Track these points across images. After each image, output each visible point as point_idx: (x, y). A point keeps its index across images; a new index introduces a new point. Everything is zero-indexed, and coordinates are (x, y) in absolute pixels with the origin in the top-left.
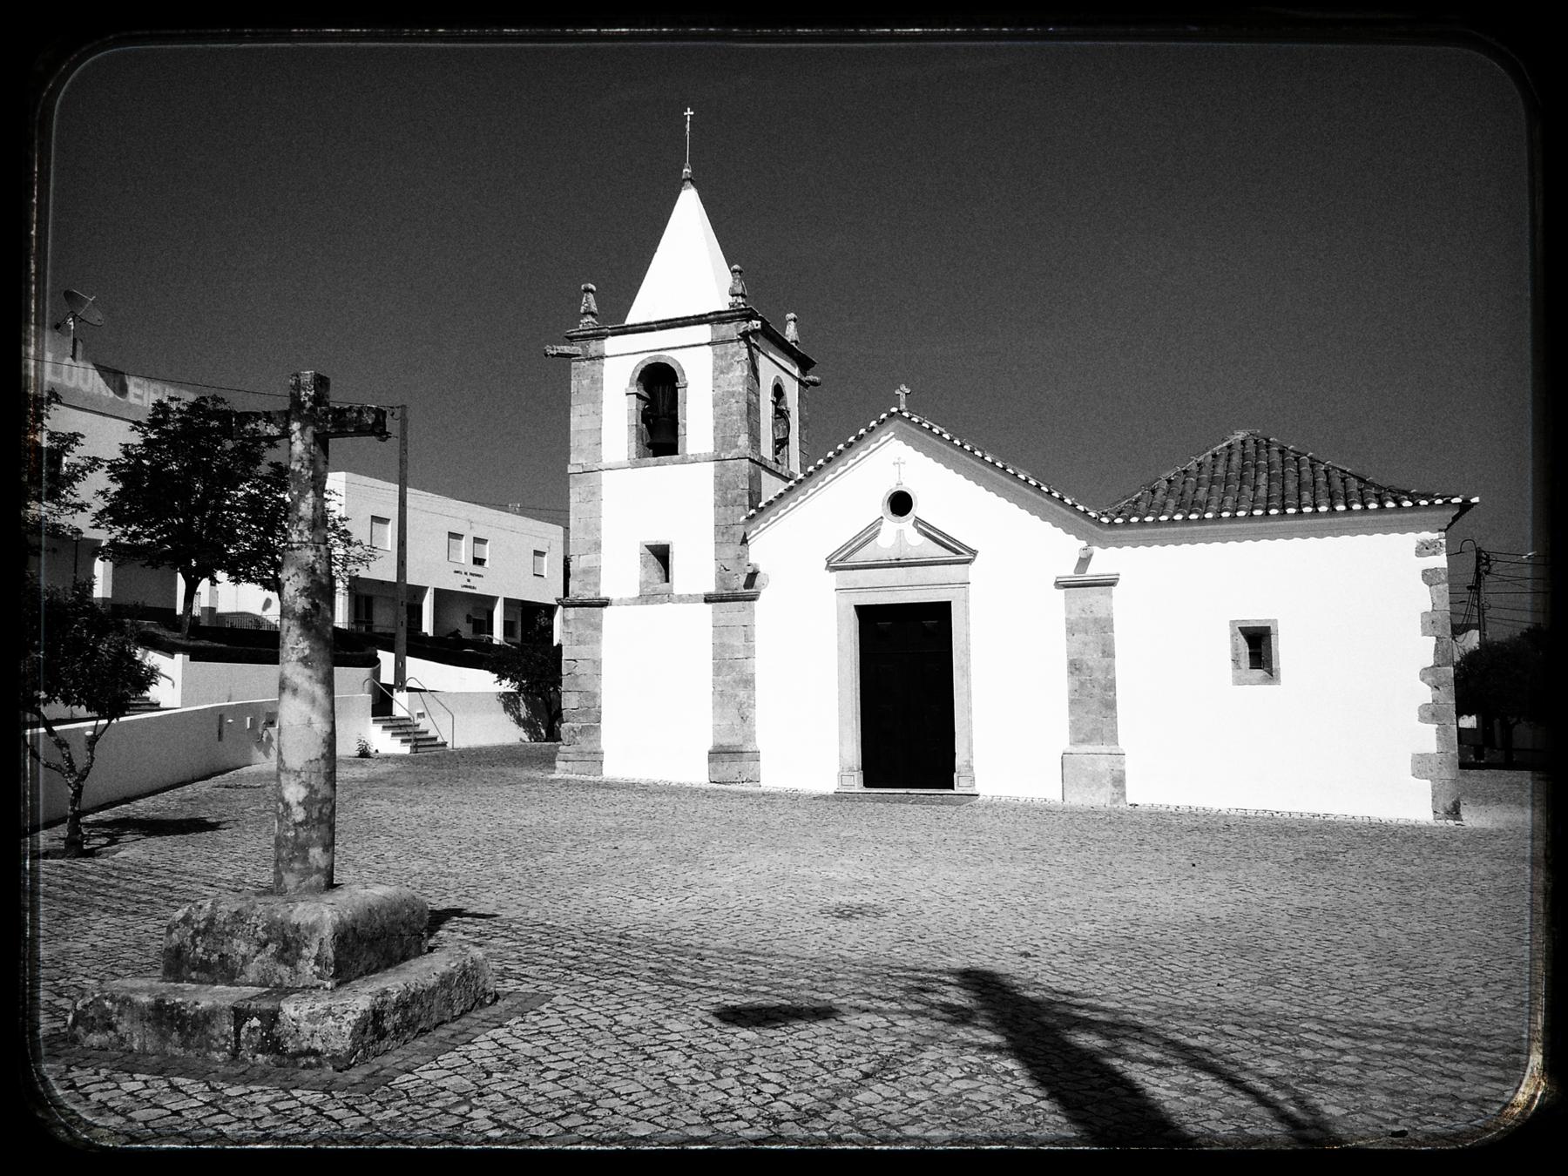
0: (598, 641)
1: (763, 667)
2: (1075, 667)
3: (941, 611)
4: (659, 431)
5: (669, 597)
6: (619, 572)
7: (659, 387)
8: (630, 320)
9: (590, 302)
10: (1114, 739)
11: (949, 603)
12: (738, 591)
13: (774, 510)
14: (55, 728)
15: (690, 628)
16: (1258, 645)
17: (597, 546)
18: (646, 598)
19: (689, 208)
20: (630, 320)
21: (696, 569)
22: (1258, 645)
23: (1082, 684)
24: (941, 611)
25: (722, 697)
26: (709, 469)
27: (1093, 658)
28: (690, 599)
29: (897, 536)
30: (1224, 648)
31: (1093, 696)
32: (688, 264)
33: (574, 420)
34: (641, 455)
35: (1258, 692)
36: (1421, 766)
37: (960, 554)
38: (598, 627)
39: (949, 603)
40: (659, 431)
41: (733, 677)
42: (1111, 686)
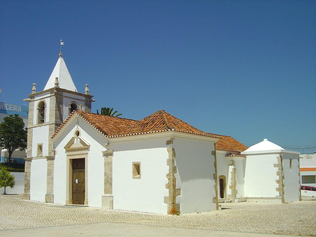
0: (30, 168)
8: (45, 89)
9: (34, 88)
16: (137, 168)
22: (137, 168)
30: (130, 168)
37: (86, 147)
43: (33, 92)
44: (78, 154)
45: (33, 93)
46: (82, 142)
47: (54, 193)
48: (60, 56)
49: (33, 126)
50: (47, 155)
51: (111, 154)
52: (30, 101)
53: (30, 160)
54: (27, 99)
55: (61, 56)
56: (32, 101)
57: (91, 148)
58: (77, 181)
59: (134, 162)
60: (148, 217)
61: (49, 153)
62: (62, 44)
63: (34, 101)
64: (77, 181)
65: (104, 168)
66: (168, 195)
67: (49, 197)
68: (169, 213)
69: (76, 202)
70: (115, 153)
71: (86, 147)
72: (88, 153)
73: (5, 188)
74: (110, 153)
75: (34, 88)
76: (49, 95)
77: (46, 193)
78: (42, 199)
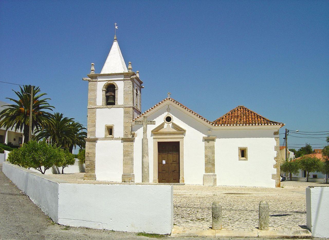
0: (95, 149)
2: (206, 156)
3: (178, 143)
4: (110, 100)
6: (100, 132)
7: (111, 89)
8: (102, 73)
9: (93, 68)
10: (214, 172)
12: (128, 140)
13: (225, 236)
14: (81, 128)
15: (117, 147)
16: (243, 153)
17: (95, 126)
18: (105, 138)
19: (115, 46)
21: (119, 132)
22: (243, 153)
23: (208, 160)
24: (178, 143)
25: (125, 164)
26: (122, 110)
27: (210, 154)
29: (168, 127)
30: (237, 153)
31: (210, 164)
32: (115, 62)
33: (89, 95)
34: (246, 149)
35: (243, 162)
36: (273, 177)
37: (182, 132)
38: (95, 145)
40: (110, 100)
41: (128, 156)
42: (214, 160)
43: (92, 72)
44: (170, 138)
45: (92, 73)
46: (175, 126)
47: (134, 173)
48: (115, 39)
49: (96, 107)
50: (122, 136)
51: (213, 140)
52: (89, 81)
53: (95, 140)
55: (116, 39)
56: (91, 82)
57: (187, 133)
58: (164, 162)
59: (240, 147)
60: (272, 189)
61: (125, 135)
62: (116, 27)
63: (96, 81)
64: (164, 162)
65: (204, 151)
66: (275, 173)
68: (277, 186)
69: (163, 181)
70: (217, 140)
71: (182, 132)
72: (184, 138)
73: (63, 168)
74: (211, 138)
75: (93, 68)
76: (122, 79)
77: (122, 174)
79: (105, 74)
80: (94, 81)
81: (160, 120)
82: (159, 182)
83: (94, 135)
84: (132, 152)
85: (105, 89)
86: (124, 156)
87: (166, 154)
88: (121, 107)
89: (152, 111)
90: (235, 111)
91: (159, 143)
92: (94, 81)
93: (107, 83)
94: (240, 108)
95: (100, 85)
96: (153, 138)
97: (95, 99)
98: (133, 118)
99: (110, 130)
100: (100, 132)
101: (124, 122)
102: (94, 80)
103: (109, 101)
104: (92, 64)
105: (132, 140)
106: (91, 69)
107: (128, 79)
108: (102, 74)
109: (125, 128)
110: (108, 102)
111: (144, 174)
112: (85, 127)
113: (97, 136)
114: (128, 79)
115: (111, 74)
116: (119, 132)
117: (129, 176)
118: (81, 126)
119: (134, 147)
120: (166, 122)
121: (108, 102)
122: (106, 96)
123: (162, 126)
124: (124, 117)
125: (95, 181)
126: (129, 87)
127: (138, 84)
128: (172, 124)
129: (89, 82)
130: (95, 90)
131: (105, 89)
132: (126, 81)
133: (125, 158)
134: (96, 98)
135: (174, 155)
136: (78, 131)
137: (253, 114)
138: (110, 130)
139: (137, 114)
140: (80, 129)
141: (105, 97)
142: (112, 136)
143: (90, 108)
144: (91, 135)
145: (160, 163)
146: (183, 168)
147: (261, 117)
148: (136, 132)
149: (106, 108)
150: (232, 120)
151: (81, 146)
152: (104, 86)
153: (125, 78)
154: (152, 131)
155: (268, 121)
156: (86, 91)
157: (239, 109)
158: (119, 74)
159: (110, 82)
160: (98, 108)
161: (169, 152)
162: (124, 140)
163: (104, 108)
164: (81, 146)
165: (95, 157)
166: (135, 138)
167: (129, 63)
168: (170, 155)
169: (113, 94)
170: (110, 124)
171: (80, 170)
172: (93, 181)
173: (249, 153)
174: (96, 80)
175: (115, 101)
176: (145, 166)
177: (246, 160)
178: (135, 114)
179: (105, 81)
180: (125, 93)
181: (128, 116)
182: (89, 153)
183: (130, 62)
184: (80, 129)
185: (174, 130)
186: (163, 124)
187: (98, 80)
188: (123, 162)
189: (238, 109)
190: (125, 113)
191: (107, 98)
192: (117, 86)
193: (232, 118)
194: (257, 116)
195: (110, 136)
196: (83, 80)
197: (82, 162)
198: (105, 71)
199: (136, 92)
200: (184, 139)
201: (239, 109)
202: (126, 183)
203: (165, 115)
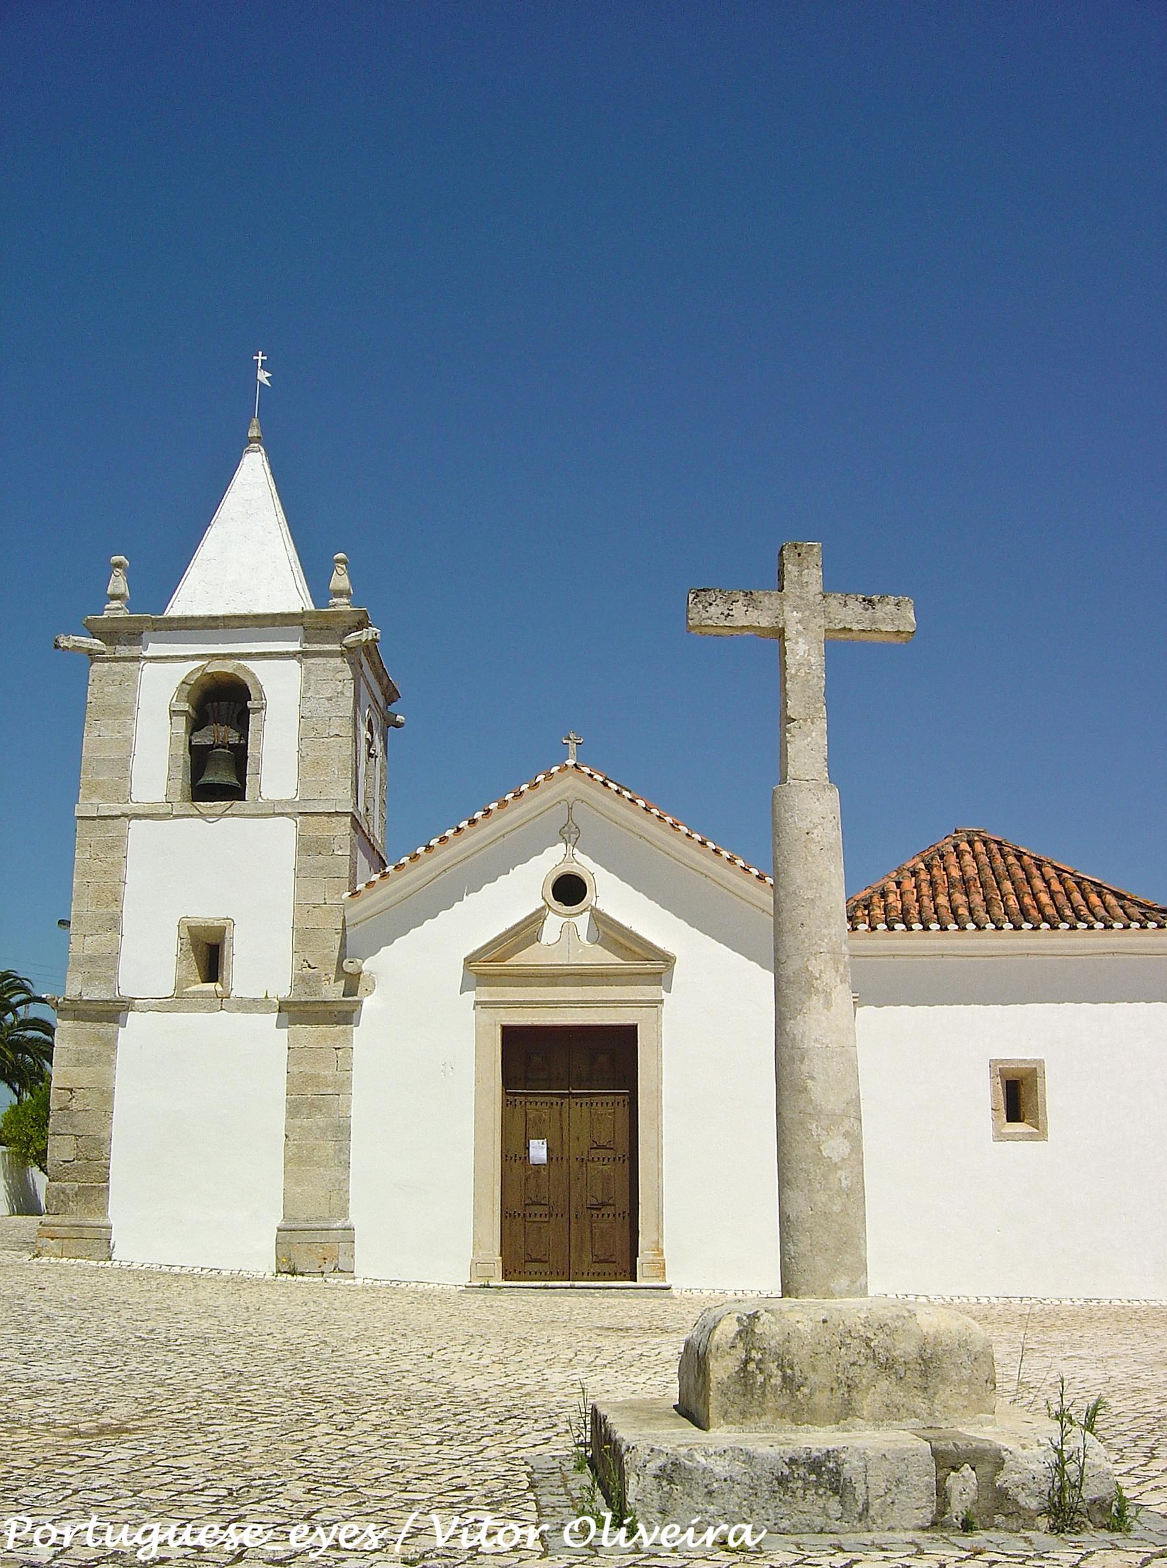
0: (111, 1062)
1: (364, 1107)
3: (627, 1036)
4: (217, 768)
5: (222, 1001)
6: (149, 960)
7: (221, 707)
8: (178, 607)
9: (118, 584)
11: (634, 1028)
12: (323, 1009)
15: (246, 1052)
16: (1018, 1096)
17: (114, 923)
18: (178, 1001)
19: (253, 474)
20: (178, 607)
21: (263, 961)
22: (1018, 1096)
24: (627, 1036)
25: (298, 1159)
26: (285, 831)
28: (249, 1005)
29: (564, 937)
30: (985, 1095)
32: (246, 553)
33: (89, 737)
35: (1020, 1151)
37: (650, 965)
38: (111, 1043)
39: (634, 1028)
40: (217, 768)
41: (317, 1116)
43: (115, 604)
44: (578, 1002)
45: (115, 610)
46: (609, 932)
47: (353, 1219)
50: (282, 989)
52: (93, 656)
53: (113, 1012)
54: (89, 640)
55: (257, 440)
56: (108, 660)
57: (679, 972)
58: (538, 1151)
61: (301, 980)
62: (263, 376)
63: (136, 659)
64: (538, 1151)
67: (311, 1243)
71: (650, 965)
75: (118, 584)
76: (295, 647)
77: (278, 1220)
78: (248, 1244)
79: (193, 618)
80: (125, 659)
81: (522, 890)
82: (505, 1277)
83: (111, 979)
84: (343, 1086)
85: (186, 707)
86: (294, 1110)
87: (547, 1099)
88: (282, 814)
89: (472, 839)
90: (942, 857)
91: (512, 1036)
92: (125, 659)
93: (197, 669)
94: (971, 843)
95: (157, 687)
96: (477, 1003)
97: (123, 765)
98: (353, 882)
99: (209, 954)
100: (149, 960)
101: (297, 905)
102: (123, 651)
103: (208, 778)
104: (116, 559)
105: (344, 1015)
106: (108, 592)
107: (328, 647)
108: (172, 619)
109: (303, 937)
110: (202, 781)
111: (822, 1197)
112: (44, 996)
113: (127, 987)
114: (328, 647)
115: (225, 617)
116: (263, 961)
117: (319, 1237)
118: (26, 990)
119: (357, 1056)
120: (556, 905)
121: (202, 781)
122: (193, 749)
123: (527, 932)
124: (298, 871)
125: (109, 1263)
126: (330, 699)
127: (381, 698)
128: (592, 916)
129: (93, 661)
130: (125, 711)
131: (186, 707)
132: (312, 661)
133: (297, 1122)
134: (130, 754)
135: (600, 1110)
136: (12, 1008)
137: (1050, 873)
138: (209, 954)
139: (380, 852)
140: (20, 1004)
141: (182, 750)
142: (219, 988)
143: (93, 818)
144: (89, 980)
145: (513, 1156)
146: (659, 1189)
147: (1100, 885)
148: (367, 965)
149: (192, 816)
150: (942, 900)
151: (17, 1086)
152: (179, 690)
153: (307, 640)
154: (469, 961)
155: (1149, 908)
156: (72, 713)
157: (964, 846)
158: (274, 616)
159: (215, 667)
160: (137, 816)
161: (571, 1084)
162: (293, 1012)
163: (176, 817)
164: (17, 1086)
165: (108, 1114)
166: (360, 1003)
167: (338, 561)
168: (575, 1111)
169: (234, 738)
170: (206, 913)
171: (10, 1204)
172: (93, 1263)
173: (1054, 1096)
174: (135, 651)
175: (241, 775)
176: (821, 1092)
177: (1039, 1132)
178: (363, 862)
179: (186, 658)
180: (310, 728)
181: (322, 868)
182: (71, 1090)
183: (341, 555)
184: (20, 1004)
185: (605, 958)
186: (534, 922)
187: (145, 654)
188: (286, 1145)
189: (956, 847)
190: (307, 846)
191: (199, 758)
192: (261, 691)
193: (940, 889)
194: (1078, 884)
195: (210, 986)
196: (57, 647)
197: (26, 1156)
198: (188, 600)
199: (369, 736)
200: (665, 1009)
201: (964, 846)
202: (300, 1278)
203: (552, 861)
